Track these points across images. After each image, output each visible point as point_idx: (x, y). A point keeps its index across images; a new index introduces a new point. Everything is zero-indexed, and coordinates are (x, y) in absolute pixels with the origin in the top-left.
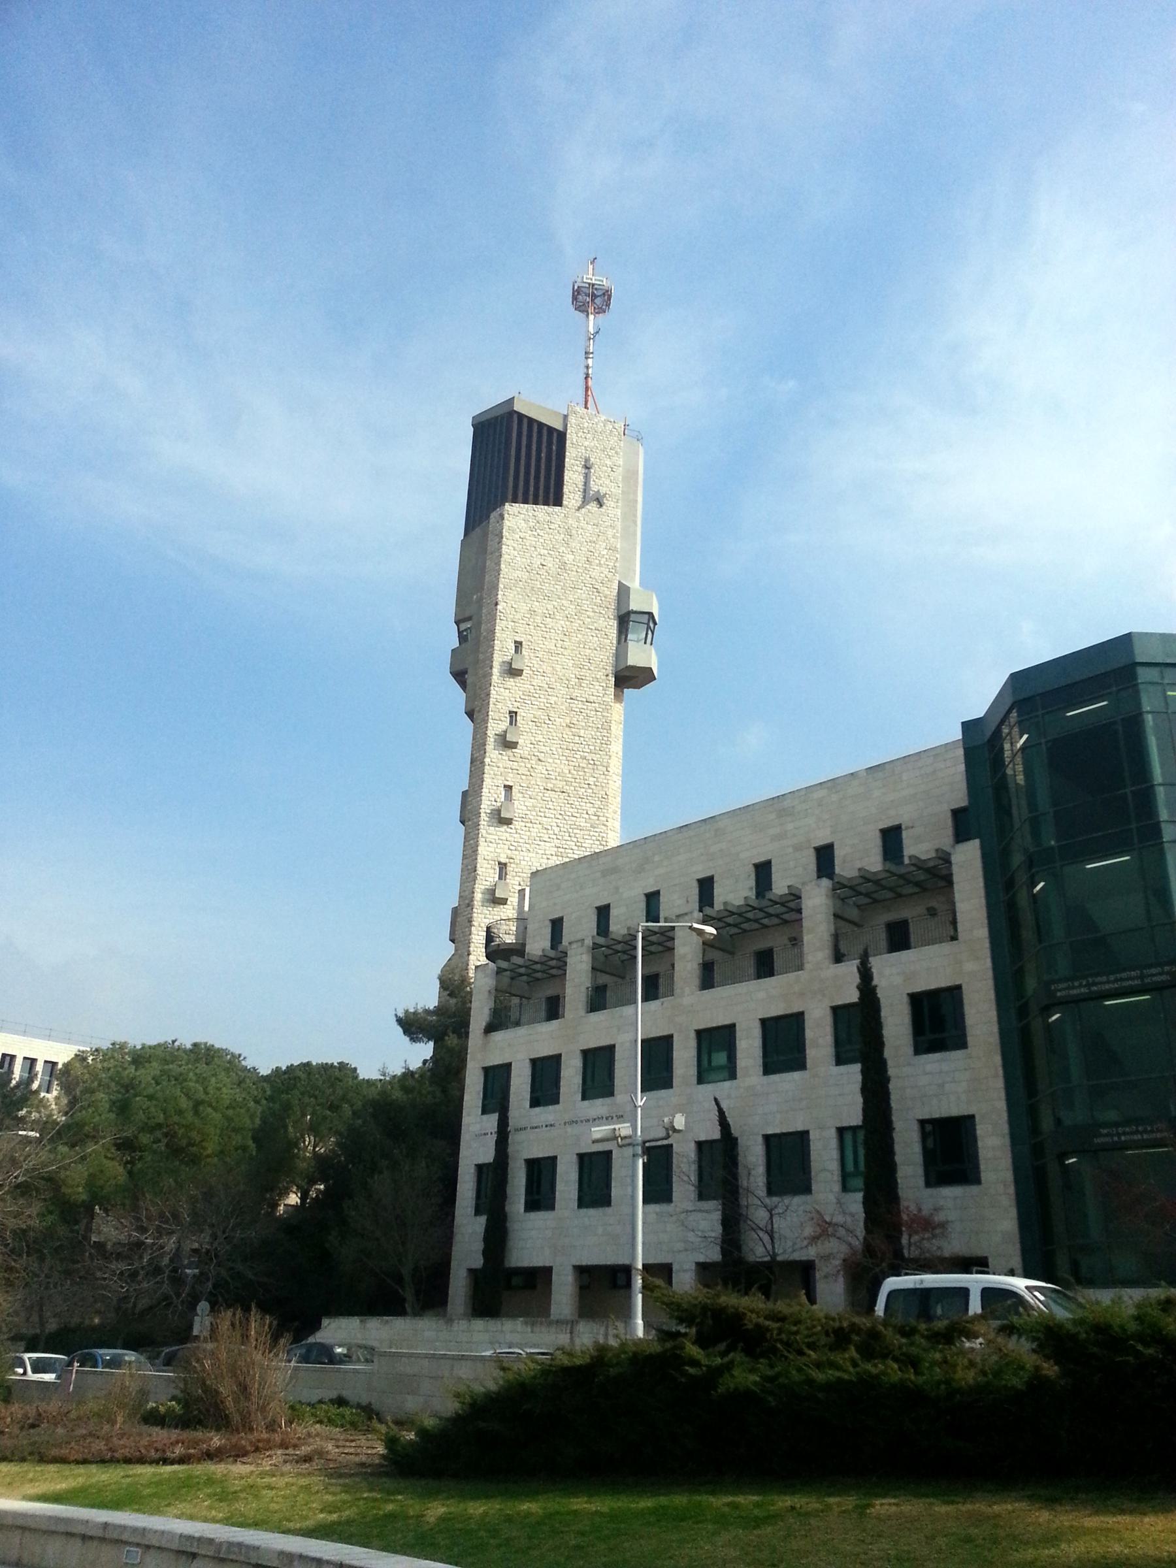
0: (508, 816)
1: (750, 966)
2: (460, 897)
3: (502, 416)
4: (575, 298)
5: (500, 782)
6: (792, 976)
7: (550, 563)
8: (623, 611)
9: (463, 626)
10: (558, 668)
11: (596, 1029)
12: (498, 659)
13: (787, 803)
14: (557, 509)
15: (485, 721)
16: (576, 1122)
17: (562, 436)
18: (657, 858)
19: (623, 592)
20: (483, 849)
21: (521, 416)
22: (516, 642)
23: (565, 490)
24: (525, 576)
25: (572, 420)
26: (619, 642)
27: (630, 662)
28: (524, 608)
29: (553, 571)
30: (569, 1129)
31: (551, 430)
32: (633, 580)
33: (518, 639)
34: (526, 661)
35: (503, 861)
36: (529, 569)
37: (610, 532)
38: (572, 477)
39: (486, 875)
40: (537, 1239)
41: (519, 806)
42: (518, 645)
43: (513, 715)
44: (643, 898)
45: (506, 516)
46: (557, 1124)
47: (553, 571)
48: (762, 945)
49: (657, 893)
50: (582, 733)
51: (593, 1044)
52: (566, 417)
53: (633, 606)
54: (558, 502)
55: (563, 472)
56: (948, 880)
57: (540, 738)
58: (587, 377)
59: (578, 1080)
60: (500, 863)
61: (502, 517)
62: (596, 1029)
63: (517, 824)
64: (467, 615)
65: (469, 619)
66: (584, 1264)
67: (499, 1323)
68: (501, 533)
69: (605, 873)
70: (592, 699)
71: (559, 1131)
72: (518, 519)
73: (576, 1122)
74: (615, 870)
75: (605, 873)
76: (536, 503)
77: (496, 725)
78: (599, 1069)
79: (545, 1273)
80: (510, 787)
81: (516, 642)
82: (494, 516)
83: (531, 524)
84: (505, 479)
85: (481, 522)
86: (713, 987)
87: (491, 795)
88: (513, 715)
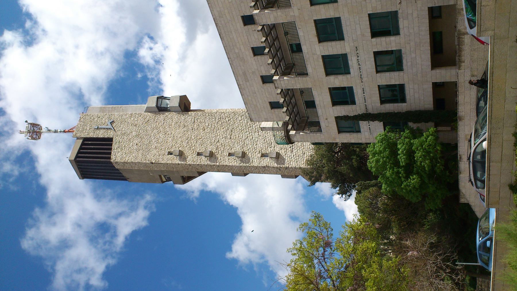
0: (241, 154)
1: (296, 56)
2: (276, 174)
3: (78, 165)
4: (34, 139)
5: (227, 158)
6: (315, 93)
7: (136, 142)
8: (156, 110)
9: (164, 180)
10: (179, 136)
11: (315, 67)
12: (177, 161)
13: (217, 14)
14: (114, 140)
15: (201, 166)
16: (361, 75)
17: (85, 139)
18: (237, 51)
19: (149, 110)
20: (256, 164)
21: (77, 157)
22: (168, 154)
23: (106, 137)
24: (141, 151)
25: (78, 135)
26: (169, 111)
27: (177, 105)
28: (155, 151)
29: (139, 140)
30: (364, 79)
31: (83, 144)
32: (144, 107)
33: (167, 153)
34: (176, 149)
35: (260, 155)
36: (138, 150)
37: (124, 117)
38: (101, 134)
39: (266, 162)
40: (419, 95)
41: (237, 149)
42: (170, 153)
43: (199, 154)
44: (256, 57)
45: (116, 161)
46: (363, 87)
47: (139, 140)
48: (287, 47)
49: (253, 49)
50: (207, 124)
51: (322, 70)
52: (78, 138)
53: (154, 105)
54: (110, 140)
55: (99, 138)
56: (273, 27)
57: (209, 142)
58: (64, 132)
59: (340, 77)
60: (262, 156)
61: (116, 163)
62: (315, 67)
63: (245, 149)
64: (158, 177)
65: (160, 176)
66: (430, 63)
67: (460, 139)
68: (123, 163)
69: (247, 80)
70: (193, 121)
71: (366, 83)
72: (118, 156)
73: (361, 75)
74: (244, 74)
75: (247, 80)
76: (111, 149)
77: (204, 161)
78: (335, 65)
79: (437, 86)
80: (229, 154)
81: (168, 154)
82: (117, 167)
83: (120, 150)
84: (102, 162)
85: (120, 173)
86: (300, 44)
87: (234, 162)
88: (199, 154)
